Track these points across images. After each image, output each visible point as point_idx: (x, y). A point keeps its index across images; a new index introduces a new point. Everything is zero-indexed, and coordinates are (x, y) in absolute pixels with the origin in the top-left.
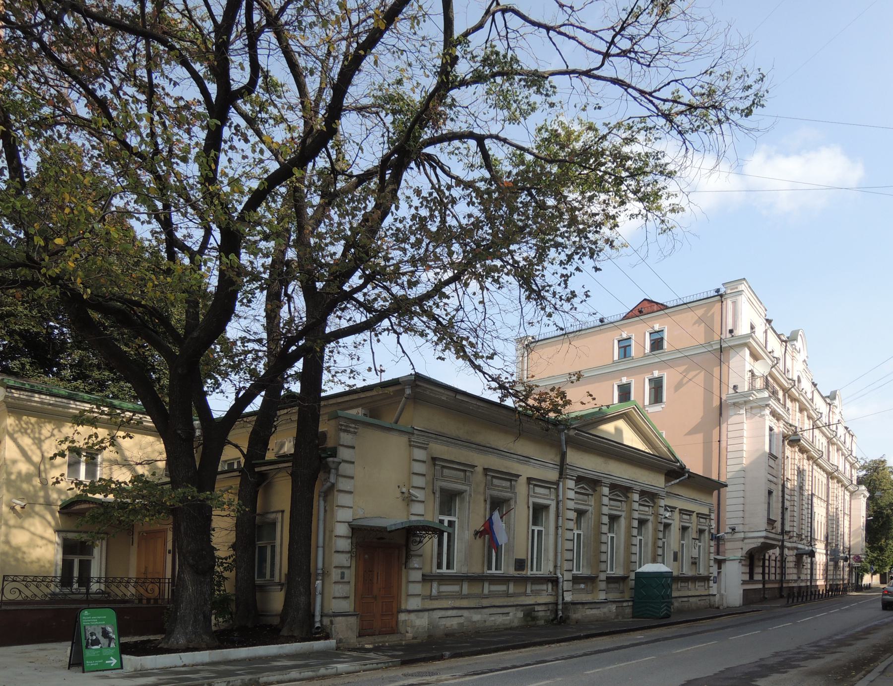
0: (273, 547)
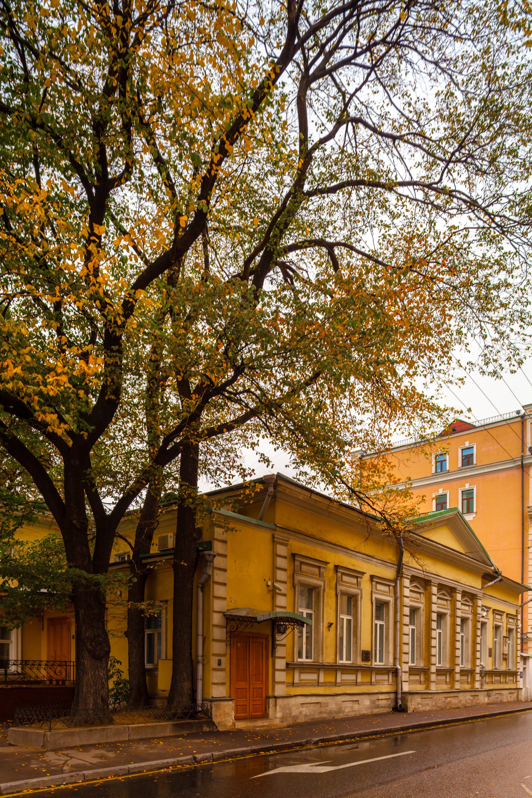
0: (159, 634)
